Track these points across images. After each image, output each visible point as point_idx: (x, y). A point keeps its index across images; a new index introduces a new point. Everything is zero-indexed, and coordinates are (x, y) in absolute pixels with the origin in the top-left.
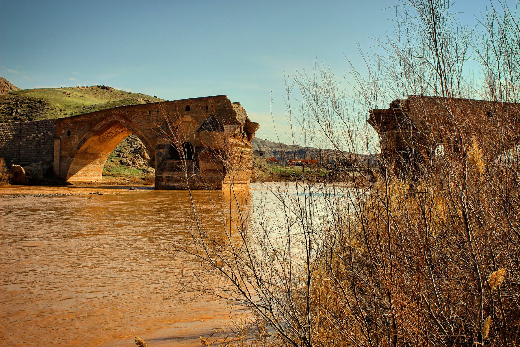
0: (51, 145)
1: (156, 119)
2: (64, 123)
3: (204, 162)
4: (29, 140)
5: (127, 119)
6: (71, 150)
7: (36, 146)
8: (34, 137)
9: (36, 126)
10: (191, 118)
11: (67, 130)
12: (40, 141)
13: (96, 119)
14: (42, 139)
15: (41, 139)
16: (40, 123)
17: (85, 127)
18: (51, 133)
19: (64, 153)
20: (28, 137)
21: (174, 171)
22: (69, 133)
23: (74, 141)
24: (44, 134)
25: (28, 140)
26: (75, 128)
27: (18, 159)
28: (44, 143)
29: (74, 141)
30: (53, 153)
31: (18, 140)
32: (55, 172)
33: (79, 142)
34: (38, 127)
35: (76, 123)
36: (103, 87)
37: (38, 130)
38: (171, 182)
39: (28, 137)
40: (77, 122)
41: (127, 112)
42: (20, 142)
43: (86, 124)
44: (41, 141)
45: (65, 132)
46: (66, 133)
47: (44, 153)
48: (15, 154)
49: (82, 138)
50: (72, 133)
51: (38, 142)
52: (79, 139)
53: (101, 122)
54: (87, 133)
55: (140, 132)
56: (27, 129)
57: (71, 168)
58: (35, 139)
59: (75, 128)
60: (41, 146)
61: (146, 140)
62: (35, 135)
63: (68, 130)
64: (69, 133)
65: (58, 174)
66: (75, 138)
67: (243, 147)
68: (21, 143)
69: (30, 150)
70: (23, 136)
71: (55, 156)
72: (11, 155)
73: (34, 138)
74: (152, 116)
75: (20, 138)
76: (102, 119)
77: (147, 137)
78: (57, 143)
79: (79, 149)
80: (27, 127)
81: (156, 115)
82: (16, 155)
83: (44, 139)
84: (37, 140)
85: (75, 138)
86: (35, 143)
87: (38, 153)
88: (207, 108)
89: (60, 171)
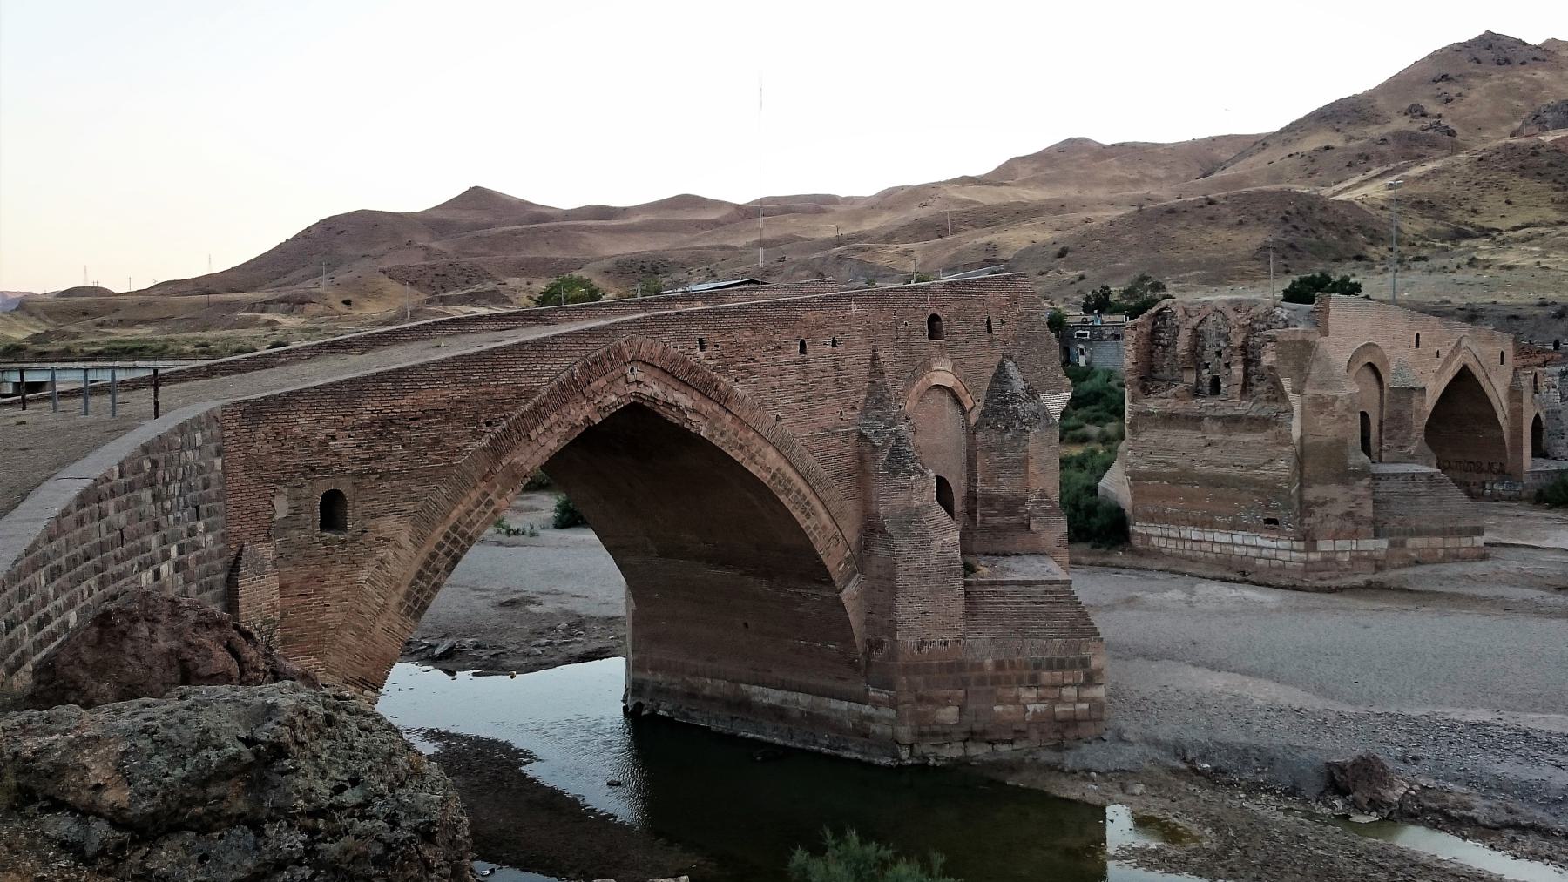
1: (836, 383)
17: (460, 451)
22: (332, 510)
26: (380, 467)
35: (385, 427)
36: (1327, 148)
49: (437, 536)
54: (474, 495)
57: (1054, 357)
59: (380, 467)
64: (332, 510)
66: (384, 541)
76: (568, 391)
79: (418, 615)
85: (384, 541)
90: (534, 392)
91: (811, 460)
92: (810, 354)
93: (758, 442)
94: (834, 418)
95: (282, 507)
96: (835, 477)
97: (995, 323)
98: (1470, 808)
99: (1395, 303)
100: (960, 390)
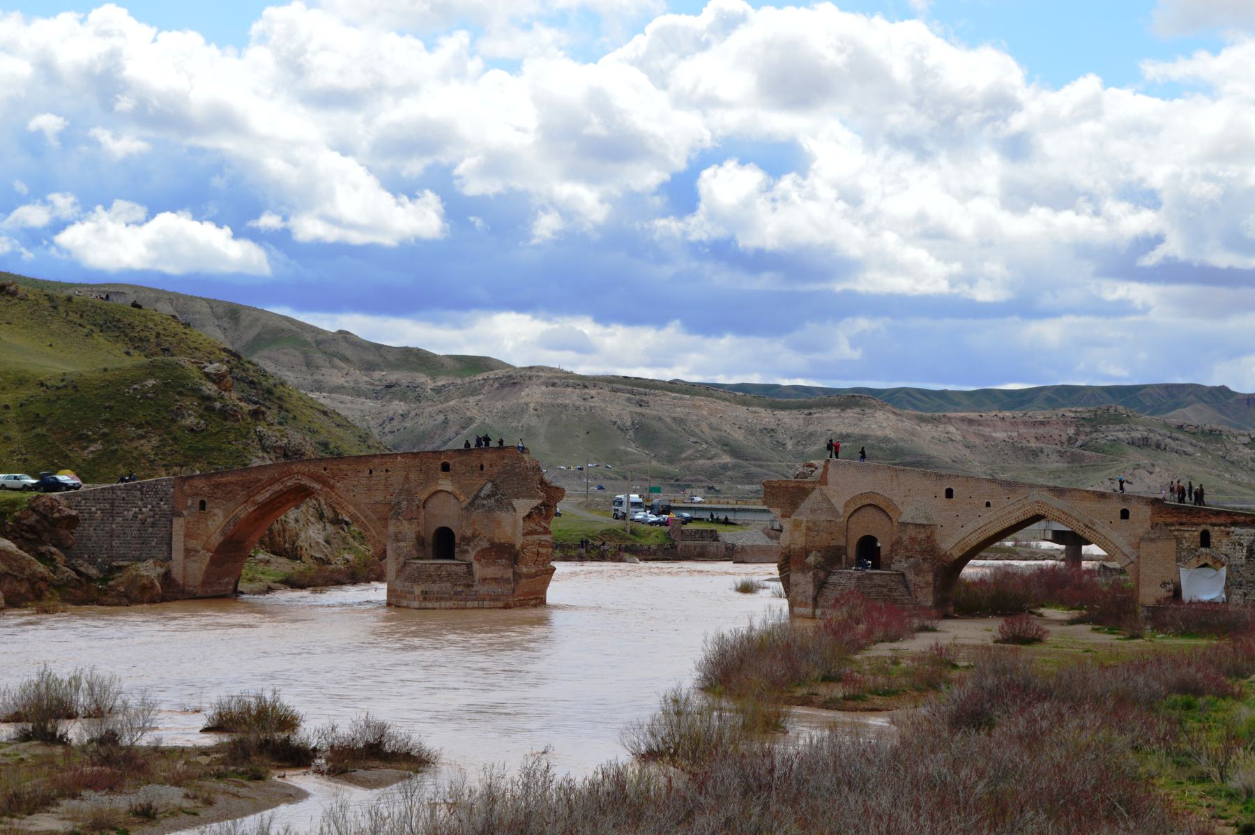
0: (166, 527)
2: (190, 486)
3: (483, 566)
4: (127, 520)
5: (324, 483)
6: (209, 538)
7: (139, 530)
8: (135, 513)
9: (139, 493)
10: (452, 485)
11: (198, 499)
12: (146, 520)
13: (259, 480)
14: (150, 517)
15: (147, 517)
16: (146, 486)
17: (238, 494)
18: (165, 504)
19: (193, 544)
20: (126, 513)
21: (434, 582)
22: (203, 505)
23: (214, 520)
24: (153, 507)
25: (125, 520)
27: (109, 557)
28: (153, 525)
29: (214, 520)
30: (170, 545)
31: (108, 519)
32: (175, 580)
33: (224, 523)
34: (142, 494)
35: (217, 485)
37: (142, 500)
38: (430, 600)
39: (126, 513)
40: (219, 484)
41: (325, 469)
42: (112, 523)
43: (239, 489)
44: (148, 520)
45: (193, 504)
46: (197, 506)
47: (153, 544)
48: (105, 546)
50: (208, 506)
51: (143, 522)
52: (225, 517)
53: (270, 485)
54: (242, 507)
55: (351, 508)
56: (124, 499)
58: (137, 517)
60: (147, 530)
61: (365, 522)
62: (137, 509)
63: (200, 499)
64: (203, 505)
65: (181, 582)
66: (214, 515)
67: (540, 533)
68: (114, 526)
69: (129, 538)
70: (117, 513)
71: (173, 548)
72: (98, 549)
73: (135, 516)
74: (374, 478)
75: (113, 517)
76: (272, 481)
77: (366, 517)
78: (178, 525)
80: (124, 495)
81: (383, 478)
82: (106, 549)
83: (153, 517)
84: (141, 520)
85: (214, 515)
86: (137, 524)
87: (143, 543)
88: (482, 468)
89: (184, 577)
90: (262, 480)
91: (369, 512)
92: (374, 474)
93: (345, 503)
94: (382, 498)
95: (189, 502)
96: (379, 519)
97: (486, 466)
98: (629, 400)
99: (993, 481)
100: (458, 493)
